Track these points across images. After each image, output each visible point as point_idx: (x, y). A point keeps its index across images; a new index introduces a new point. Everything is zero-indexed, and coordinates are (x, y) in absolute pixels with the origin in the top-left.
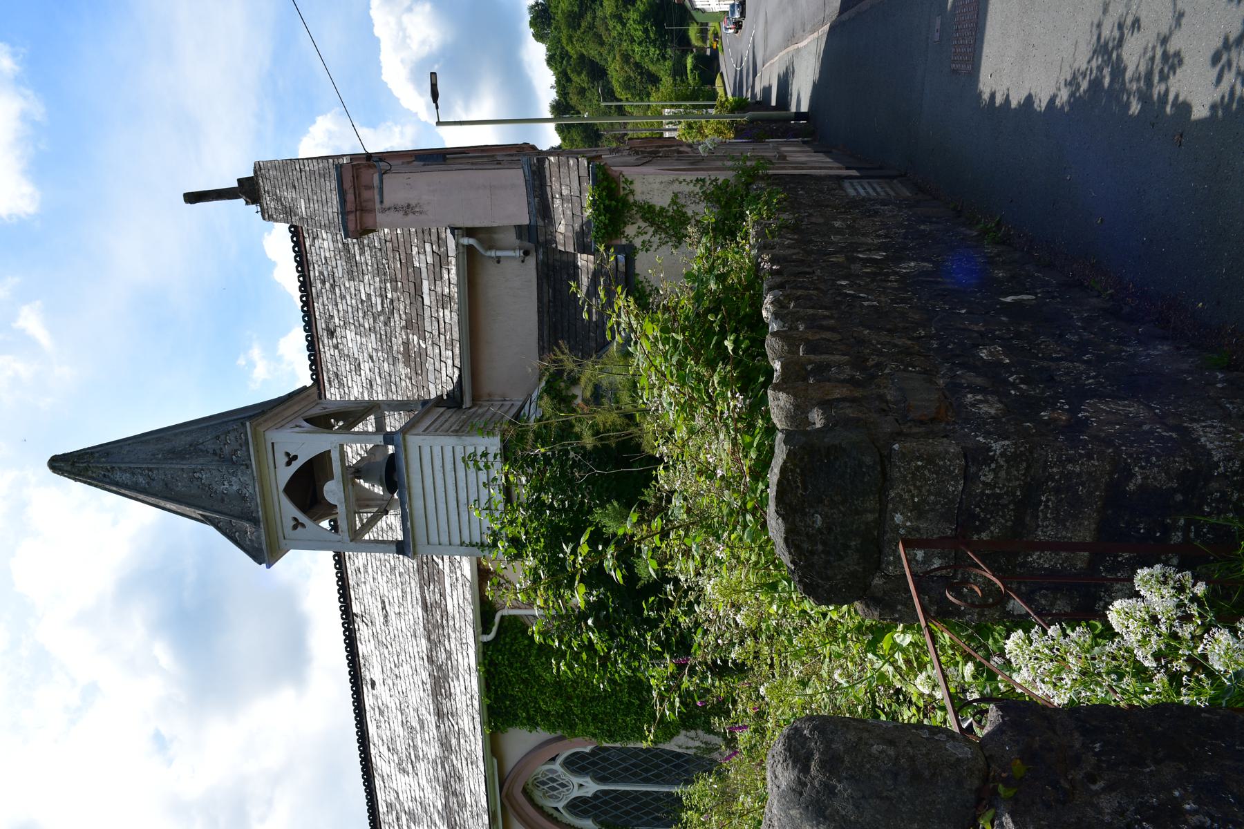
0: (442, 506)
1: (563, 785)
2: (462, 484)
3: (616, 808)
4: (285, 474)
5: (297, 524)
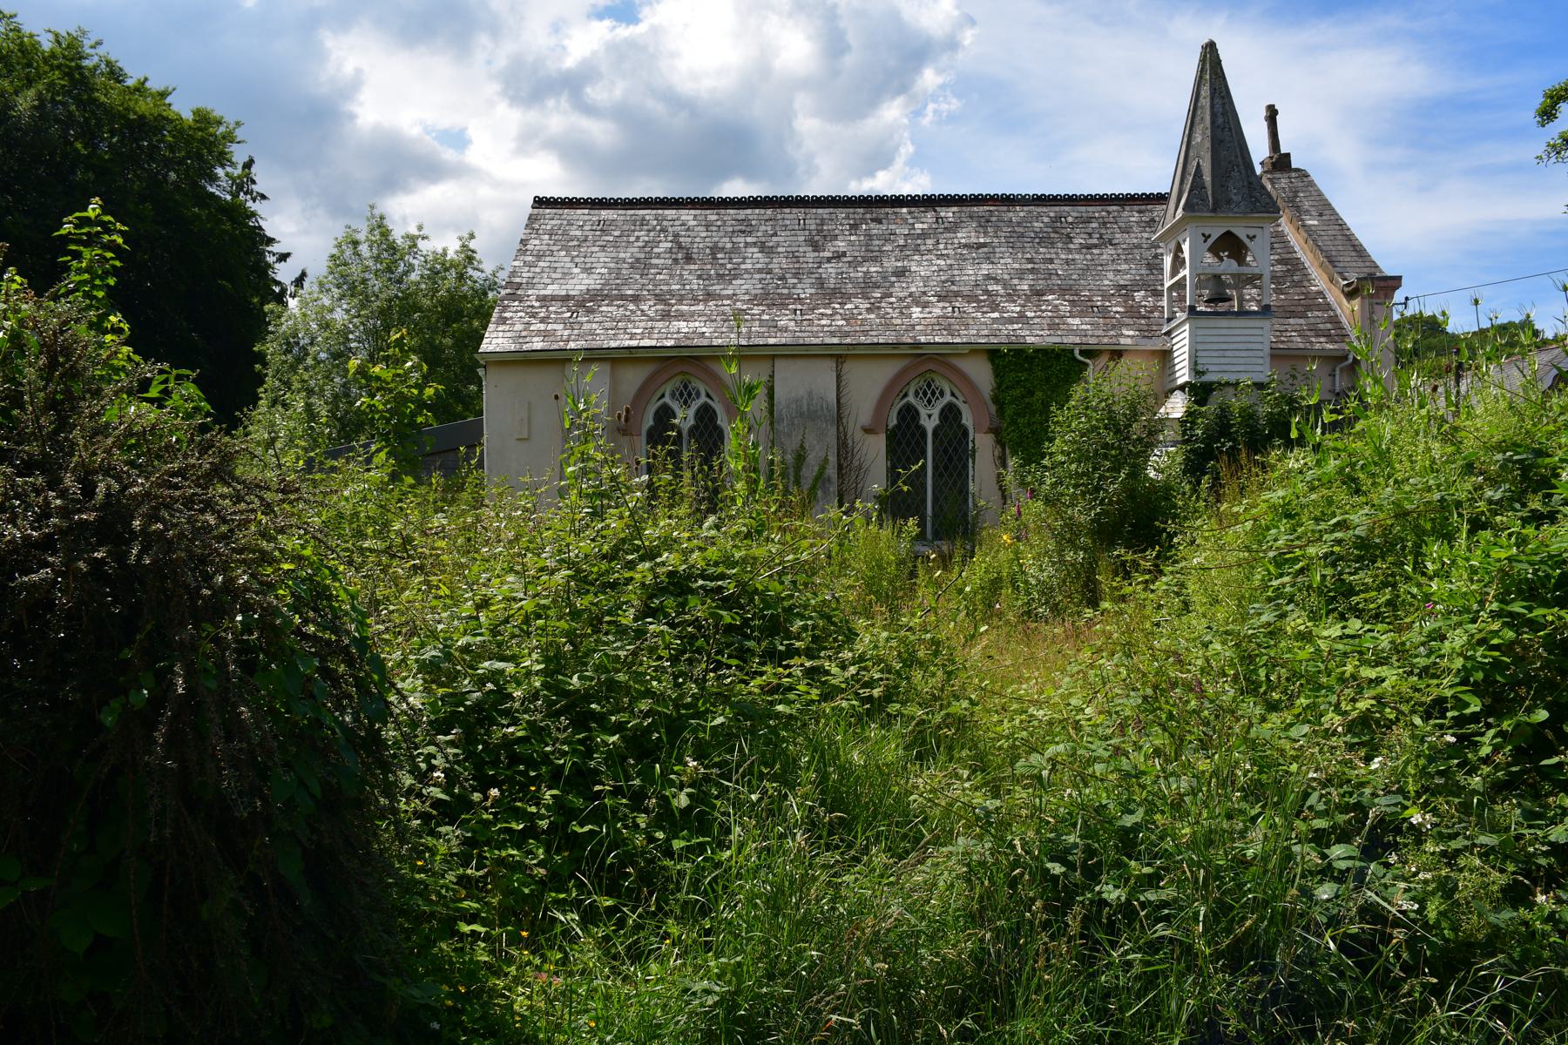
0: (1222, 339)
1: (929, 401)
2: (1237, 353)
3: (908, 444)
4: (1241, 233)
5: (1206, 237)
